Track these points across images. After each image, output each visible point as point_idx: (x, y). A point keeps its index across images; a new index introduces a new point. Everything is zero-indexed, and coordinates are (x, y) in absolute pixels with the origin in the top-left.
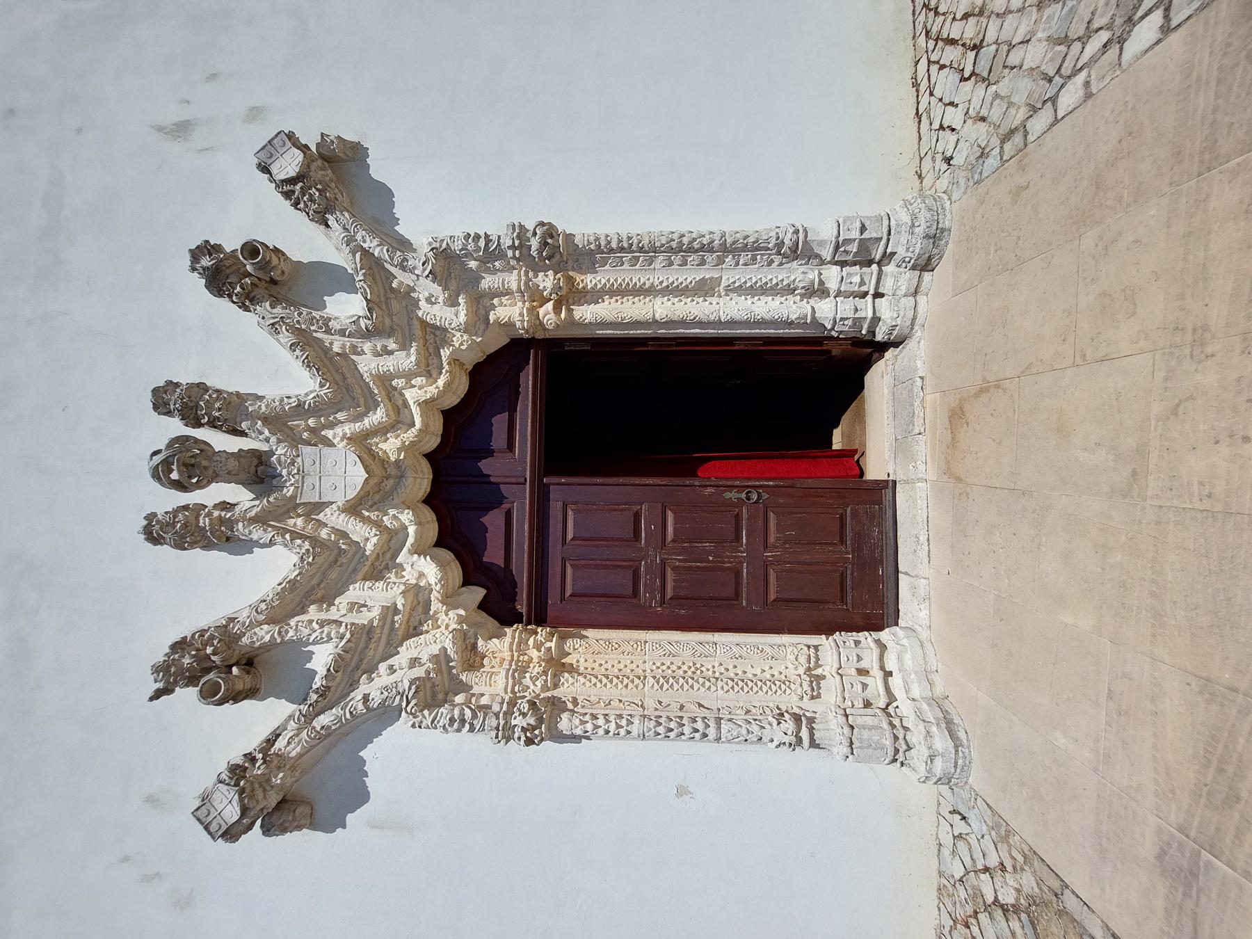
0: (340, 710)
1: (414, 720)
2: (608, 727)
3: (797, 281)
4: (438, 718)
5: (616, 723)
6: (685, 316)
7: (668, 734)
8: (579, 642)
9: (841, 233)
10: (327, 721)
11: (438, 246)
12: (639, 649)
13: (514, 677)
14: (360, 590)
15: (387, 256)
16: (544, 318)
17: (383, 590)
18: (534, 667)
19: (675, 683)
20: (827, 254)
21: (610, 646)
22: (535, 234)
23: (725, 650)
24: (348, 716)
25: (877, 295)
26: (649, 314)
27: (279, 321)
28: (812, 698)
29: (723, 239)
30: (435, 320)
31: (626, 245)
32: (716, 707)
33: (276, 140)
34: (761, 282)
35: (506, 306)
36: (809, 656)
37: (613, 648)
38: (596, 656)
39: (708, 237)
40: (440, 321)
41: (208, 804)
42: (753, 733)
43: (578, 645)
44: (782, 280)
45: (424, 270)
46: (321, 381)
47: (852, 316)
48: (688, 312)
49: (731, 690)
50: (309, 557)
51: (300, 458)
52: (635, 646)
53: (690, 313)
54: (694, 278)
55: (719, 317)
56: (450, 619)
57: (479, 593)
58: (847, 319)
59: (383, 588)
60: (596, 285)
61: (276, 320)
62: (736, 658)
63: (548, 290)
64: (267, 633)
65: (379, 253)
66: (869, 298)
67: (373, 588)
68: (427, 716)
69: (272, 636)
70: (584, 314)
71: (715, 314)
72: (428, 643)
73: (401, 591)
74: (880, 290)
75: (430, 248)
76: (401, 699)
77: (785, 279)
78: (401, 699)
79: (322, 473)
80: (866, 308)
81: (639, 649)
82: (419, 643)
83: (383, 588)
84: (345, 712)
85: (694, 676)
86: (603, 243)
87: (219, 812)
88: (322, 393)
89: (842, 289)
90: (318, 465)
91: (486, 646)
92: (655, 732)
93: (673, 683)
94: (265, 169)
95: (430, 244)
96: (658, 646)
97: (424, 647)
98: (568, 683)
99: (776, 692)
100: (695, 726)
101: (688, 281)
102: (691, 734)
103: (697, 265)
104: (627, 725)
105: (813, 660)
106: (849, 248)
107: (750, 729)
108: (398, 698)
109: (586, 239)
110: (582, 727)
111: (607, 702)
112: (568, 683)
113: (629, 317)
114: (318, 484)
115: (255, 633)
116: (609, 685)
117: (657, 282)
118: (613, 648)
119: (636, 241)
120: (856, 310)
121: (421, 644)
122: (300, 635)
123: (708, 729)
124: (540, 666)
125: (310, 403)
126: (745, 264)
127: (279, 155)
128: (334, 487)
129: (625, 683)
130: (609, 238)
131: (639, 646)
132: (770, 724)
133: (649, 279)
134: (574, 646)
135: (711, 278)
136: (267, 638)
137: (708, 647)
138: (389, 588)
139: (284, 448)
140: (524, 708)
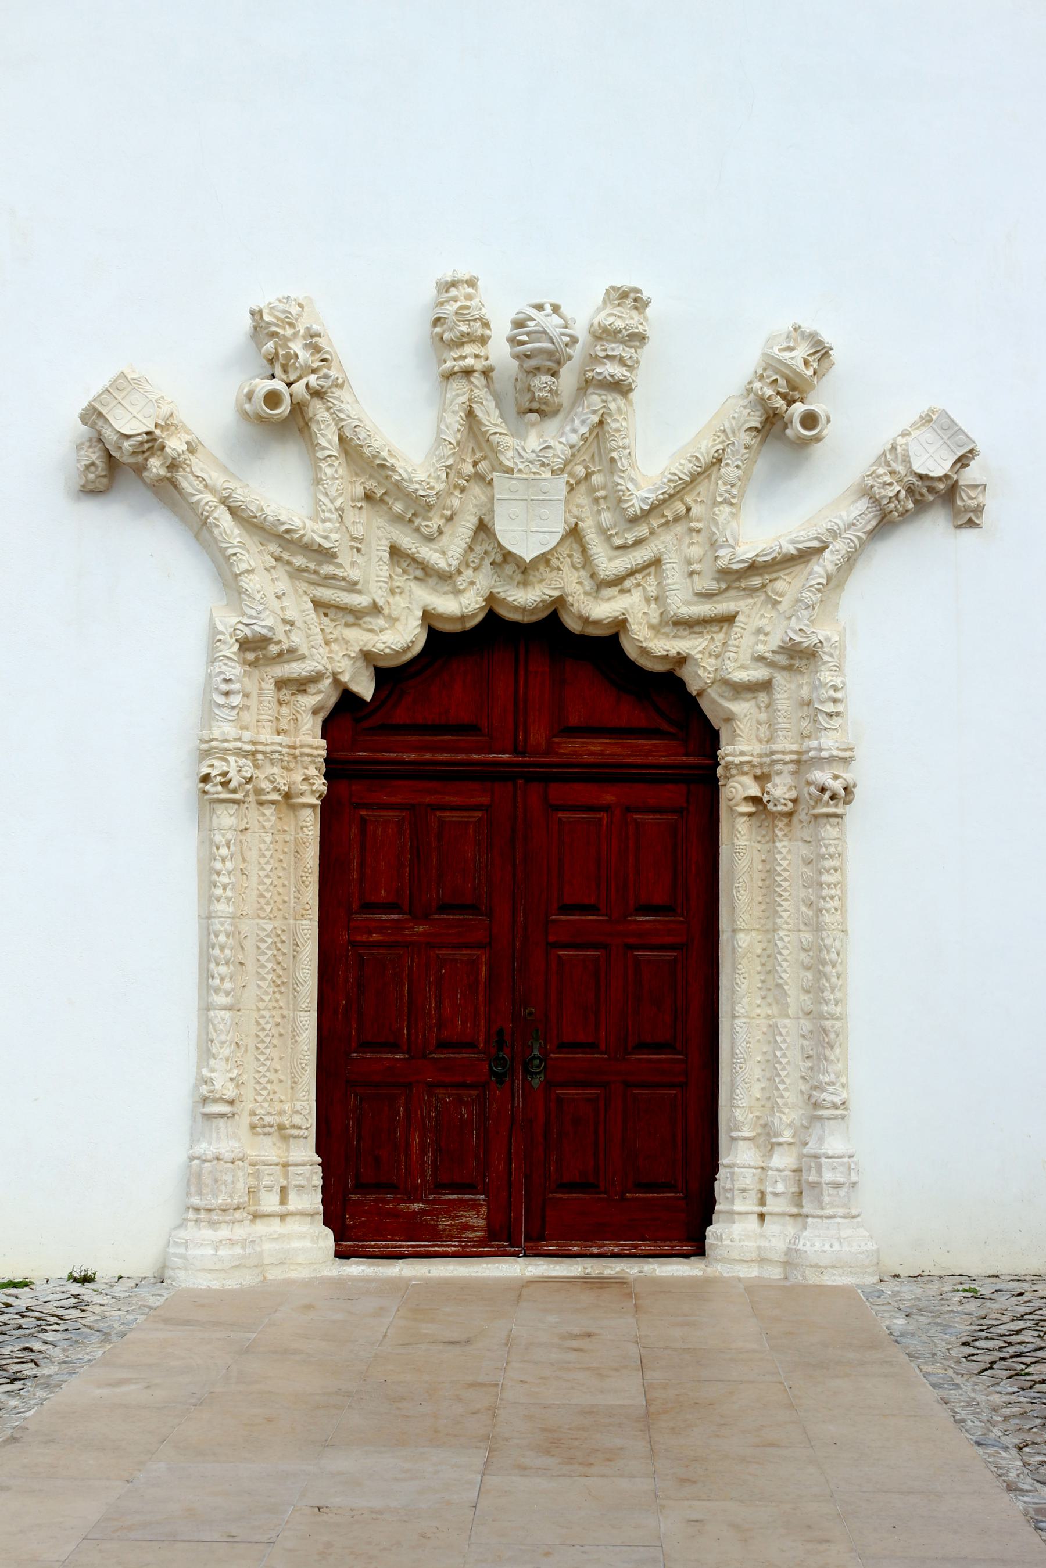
0: (239, 539)
1: (228, 634)
2: (224, 874)
3: (782, 1115)
4: (230, 663)
5: (228, 884)
6: (740, 972)
7: (217, 948)
8: (310, 833)
9: (830, 1160)
10: (225, 525)
11: (826, 650)
12: (304, 912)
13: (272, 752)
14: (378, 545)
15: (813, 583)
16: (739, 783)
17: (377, 576)
18: (283, 777)
19: (267, 957)
20: (811, 1148)
21: (307, 875)
22: (836, 777)
23: (304, 1022)
24: (231, 551)
25: (762, 1216)
26: (743, 923)
27: (729, 440)
28: (253, 1127)
29: (828, 1016)
30: (735, 639)
31: (824, 893)
32: (242, 1007)
33: (964, 437)
34: (781, 1070)
35: (758, 728)
36: (300, 1128)
37: (304, 878)
38: (292, 856)
39: (832, 997)
40: (734, 646)
41: (131, 387)
42: (221, 1048)
43: (308, 833)
44: (782, 1097)
45: (795, 632)
46: (649, 498)
47: (736, 1187)
48: (746, 975)
49: (260, 1027)
50: (424, 490)
51: (549, 475)
52: (308, 907)
53: (744, 978)
54: (786, 983)
55: (738, 1017)
56: (339, 662)
57: (365, 689)
58: (732, 1181)
59: (381, 576)
60: (780, 853)
61: (730, 435)
62: (294, 1036)
63: (773, 790)
64: (330, 442)
65: (817, 573)
66: (758, 1209)
67: (381, 563)
68: (231, 650)
69: (325, 448)
70: (744, 837)
71: (743, 1011)
72: (311, 638)
73: (377, 600)
74: (767, 1218)
75: (822, 640)
76: (250, 617)
77: (784, 1100)
78: (250, 617)
79: (531, 502)
80: (745, 1205)
81: (304, 912)
82: (310, 626)
83: (381, 576)
84: (235, 547)
85: (769, 961)
86: (828, 864)
87: (122, 402)
88: (635, 501)
89: (770, 1173)
90: (541, 498)
91: (304, 711)
92: (221, 931)
93: (266, 942)
94: (927, 420)
95: (828, 639)
96: (308, 936)
97: (306, 632)
98: (265, 821)
99: (259, 1083)
100: (227, 980)
101: (784, 975)
102: (219, 975)
103: (802, 985)
104: (226, 898)
105: (295, 1132)
106: (813, 1171)
107: (225, 1045)
108: (253, 613)
109: (831, 842)
110: (224, 843)
111: (246, 872)
112: (784, 1090)
113: (740, 897)
114: (518, 497)
115: (328, 426)
116: (262, 873)
117: (782, 933)
118: (304, 878)
119: (828, 906)
120: (744, 1191)
121: (310, 629)
122: (327, 484)
123: (223, 995)
124: (284, 784)
125: (621, 485)
126: (802, 1047)
127: (946, 438)
128: (514, 517)
129: (266, 894)
130: (832, 871)
131: (307, 912)
132: (230, 1071)
133: (787, 923)
134: (307, 827)
135: (788, 1005)
136: (324, 443)
137: (308, 1001)
138: (382, 584)
139: (563, 454)
140: (246, 771)
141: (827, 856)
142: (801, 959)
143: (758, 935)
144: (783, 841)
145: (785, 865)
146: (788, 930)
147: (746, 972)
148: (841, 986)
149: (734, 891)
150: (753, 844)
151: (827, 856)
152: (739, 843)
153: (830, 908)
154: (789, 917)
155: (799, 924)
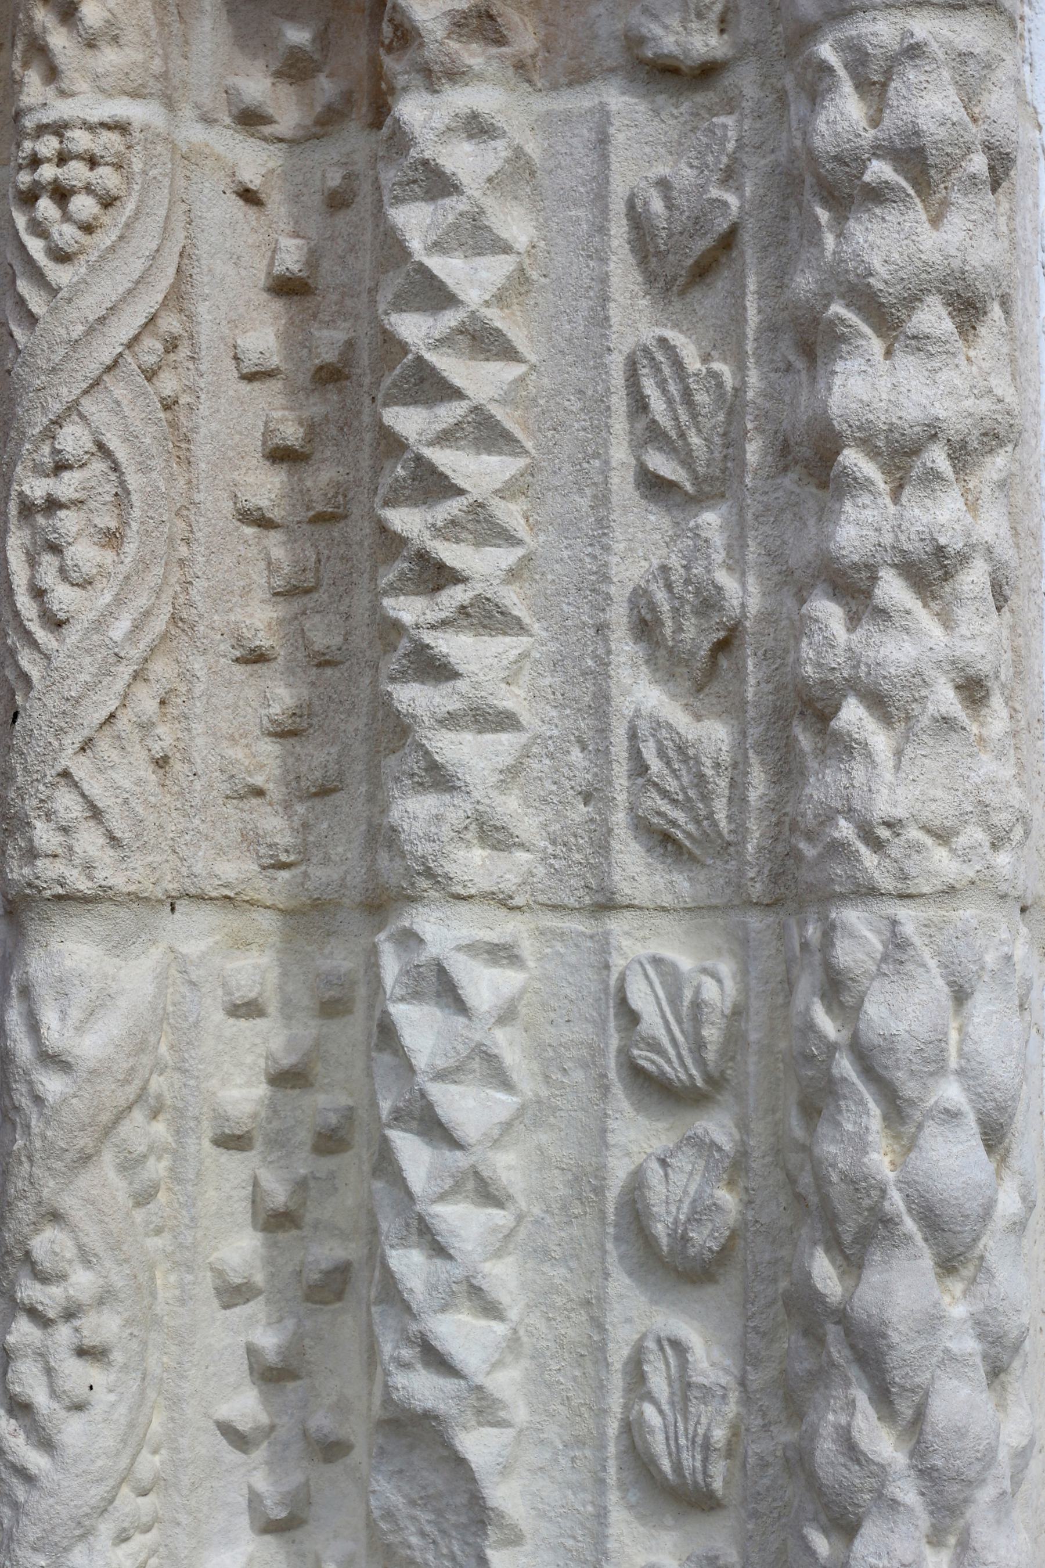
70: (109, 58)
141: (880, 170)
142: (619, 1171)
143: (240, 944)
144: (456, 75)
145: (472, 296)
146: (504, 902)
147: (104, 1298)
148: (1022, 1455)
149: (17, 541)
150: (194, 133)
151: (880, 170)
152: (62, 109)
153: (918, 679)
154: (512, 773)
155: (603, 846)
